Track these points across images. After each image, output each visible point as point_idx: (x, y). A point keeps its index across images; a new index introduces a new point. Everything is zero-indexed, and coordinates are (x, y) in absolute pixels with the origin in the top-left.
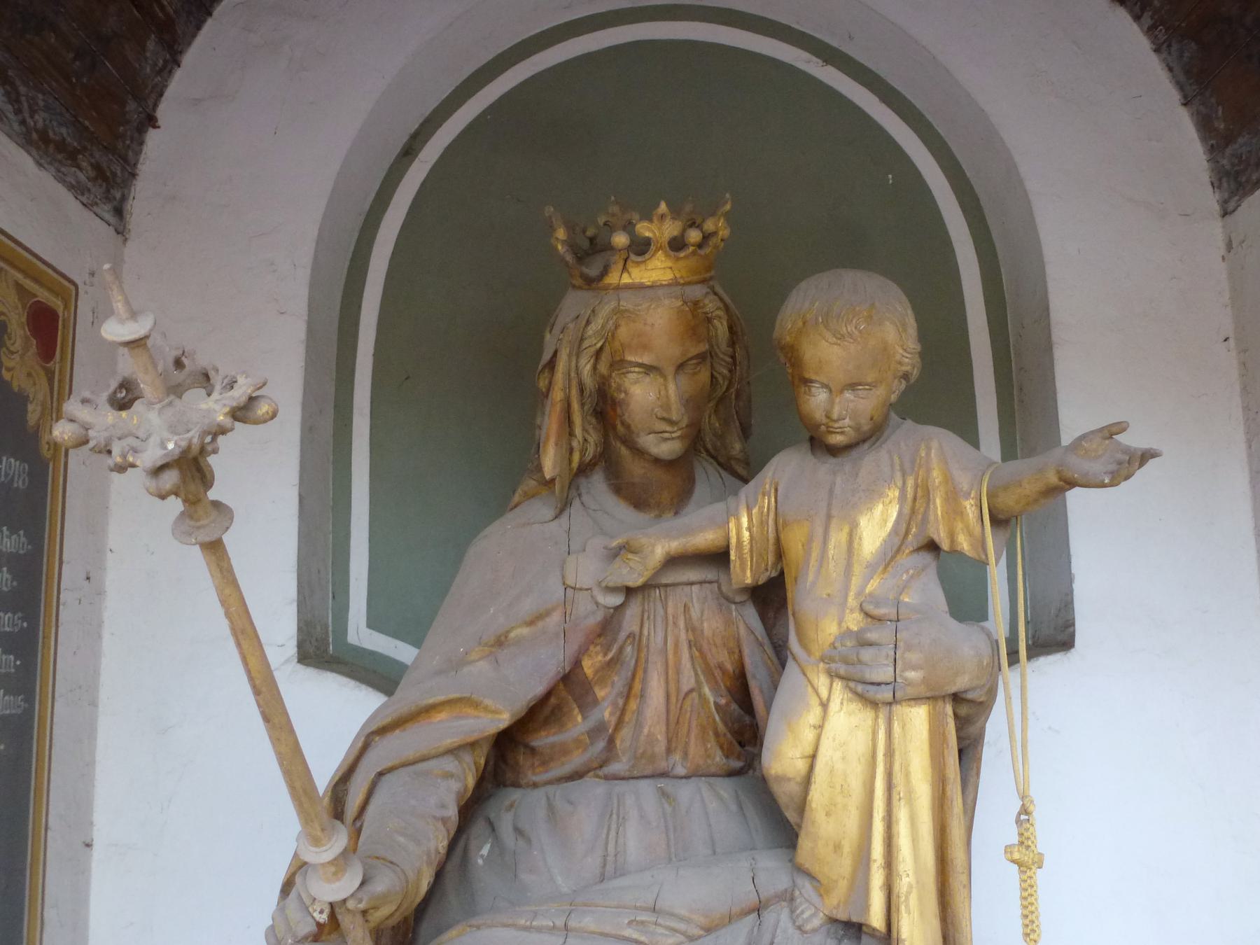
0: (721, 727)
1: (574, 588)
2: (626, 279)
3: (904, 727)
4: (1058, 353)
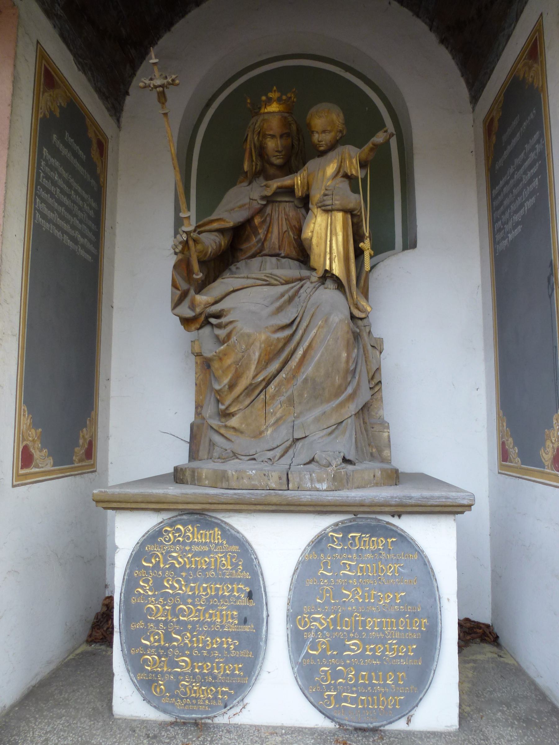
0: (295, 245)
1: (252, 200)
2: (266, 111)
3: (335, 217)
4: (415, 157)
